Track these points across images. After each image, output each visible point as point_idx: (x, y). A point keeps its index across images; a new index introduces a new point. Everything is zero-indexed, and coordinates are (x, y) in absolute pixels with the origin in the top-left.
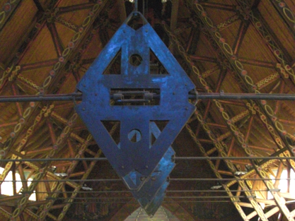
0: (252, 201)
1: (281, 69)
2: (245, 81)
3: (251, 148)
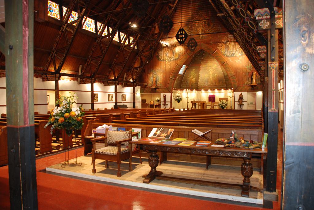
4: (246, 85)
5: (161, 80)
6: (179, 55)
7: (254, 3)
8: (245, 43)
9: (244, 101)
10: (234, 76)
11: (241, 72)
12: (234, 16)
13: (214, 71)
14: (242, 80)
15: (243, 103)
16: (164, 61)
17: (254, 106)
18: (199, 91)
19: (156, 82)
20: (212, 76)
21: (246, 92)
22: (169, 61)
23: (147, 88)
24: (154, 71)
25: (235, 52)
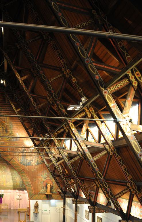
0: (50, 155)
1: (65, 71)
2: (42, 78)
3: (48, 124)
7: (117, 157)
8: (76, 177)
15: (34, 209)
21: (41, 200)
25: (31, 161)
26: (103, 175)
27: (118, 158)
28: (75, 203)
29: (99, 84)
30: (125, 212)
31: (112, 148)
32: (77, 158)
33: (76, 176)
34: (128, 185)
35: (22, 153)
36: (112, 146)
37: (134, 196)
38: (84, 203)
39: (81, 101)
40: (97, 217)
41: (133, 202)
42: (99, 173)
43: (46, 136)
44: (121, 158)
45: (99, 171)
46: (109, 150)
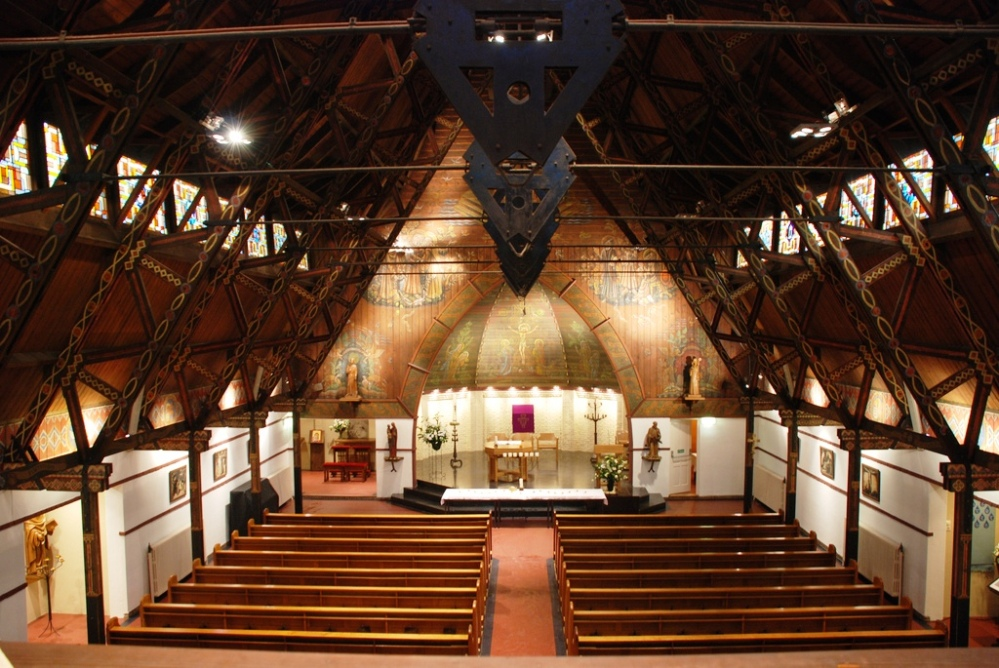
4: (669, 396)
5: (375, 373)
6: (444, 287)
7: (939, 274)
8: (801, 339)
9: (660, 446)
10: (631, 369)
11: (654, 356)
12: (877, 308)
13: (532, 328)
14: (657, 380)
16: (387, 305)
17: (686, 460)
18: (477, 392)
19: (358, 379)
20: (524, 344)
21: (668, 420)
22: (406, 307)
23: (324, 397)
24: (350, 338)
25: (634, 291)
26: (893, 326)
27: (942, 274)
28: (790, 423)
29: (896, 71)
30: (961, 440)
31: (921, 244)
32: (803, 277)
33: (799, 335)
34: (970, 357)
35: (602, 265)
36: (922, 238)
37: (991, 394)
38: (818, 425)
39: (833, 109)
40: (864, 466)
41: (986, 413)
42: (881, 321)
43: (697, 209)
44: (949, 275)
45: (881, 315)
46: (914, 251)
